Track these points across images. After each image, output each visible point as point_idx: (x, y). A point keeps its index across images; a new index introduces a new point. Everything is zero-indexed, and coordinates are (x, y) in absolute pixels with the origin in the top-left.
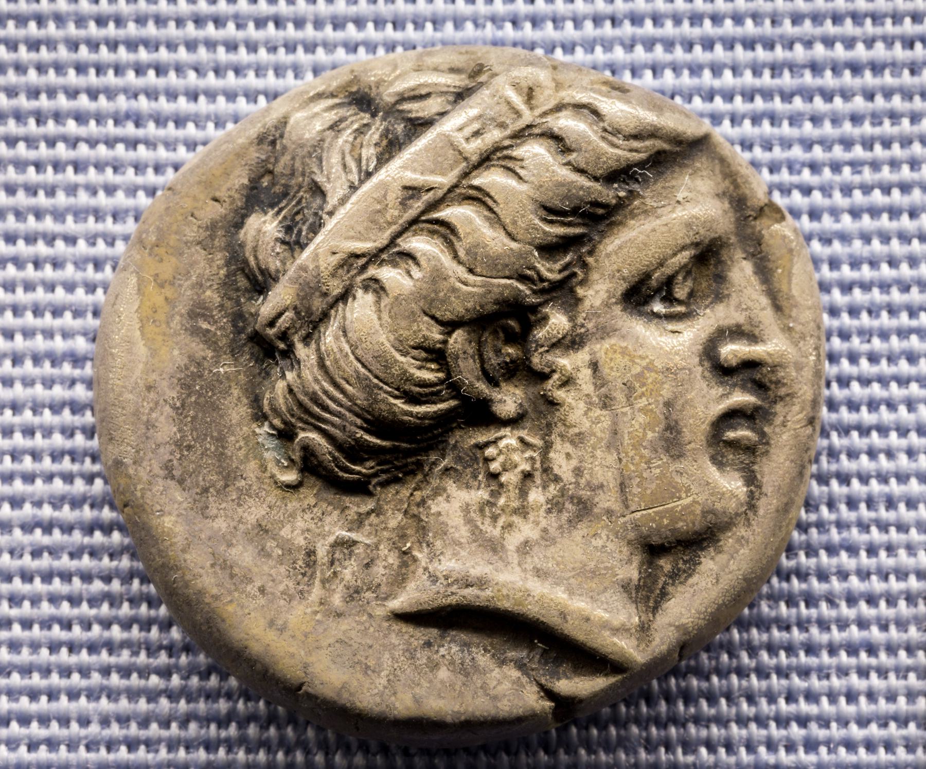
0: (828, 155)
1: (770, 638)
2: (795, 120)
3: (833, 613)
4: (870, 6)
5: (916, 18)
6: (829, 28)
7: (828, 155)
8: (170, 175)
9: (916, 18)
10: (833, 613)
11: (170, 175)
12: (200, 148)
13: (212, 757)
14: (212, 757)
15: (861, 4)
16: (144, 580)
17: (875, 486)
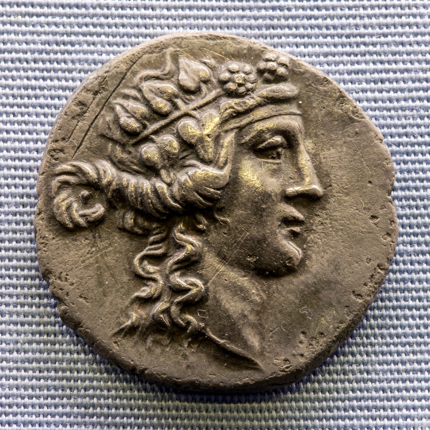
5: (425, 7)
9: (425, 7)
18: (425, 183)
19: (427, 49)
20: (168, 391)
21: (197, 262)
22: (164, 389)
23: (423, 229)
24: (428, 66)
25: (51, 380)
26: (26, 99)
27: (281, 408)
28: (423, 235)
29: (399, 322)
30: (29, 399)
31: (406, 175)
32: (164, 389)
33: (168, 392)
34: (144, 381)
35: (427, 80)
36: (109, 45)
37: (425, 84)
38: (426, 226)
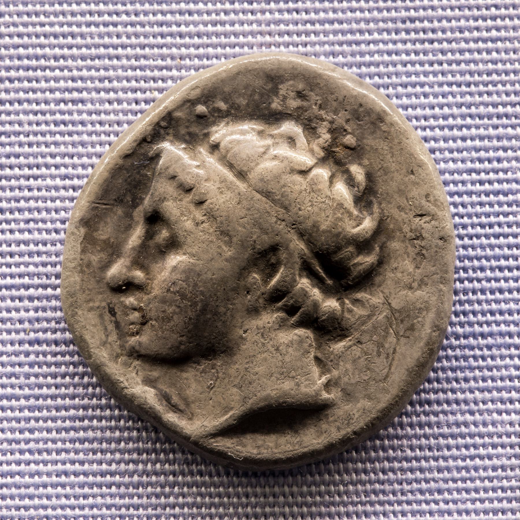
0: (504, 88)
1: (420, 398)
2: (281, 34)
3: (458, 386)
4: (458, 3)
5: (515, 7)
6: (467, 12)
7: (504, 88)
8: (90, 170)
9: (515, 7)
10: (458, 386)
11: (90, 170)
12: (165, 92)
13: (113, 435)
14: (113, 435)
15: (472, 2)
16: (85, 366)
17: (476, 284)
18: (515, 251)
19: (518, 121)
20: (237, 474)
21: (357, 200)
22: (232, 472)
23: (512, 56)
24: (518, 121)
25: (89, 442)
26: (17, 191)
27: (380, 447)
28: (513, 84)
29: (493, 318)
30: (16, 510)
31: (498, 274)
32: (232, 472)
33: (238, 477)
34: (208, 461)
35: (517, 182)
36: (351, 11)
37: (514, 120)
38: (515, 72)
